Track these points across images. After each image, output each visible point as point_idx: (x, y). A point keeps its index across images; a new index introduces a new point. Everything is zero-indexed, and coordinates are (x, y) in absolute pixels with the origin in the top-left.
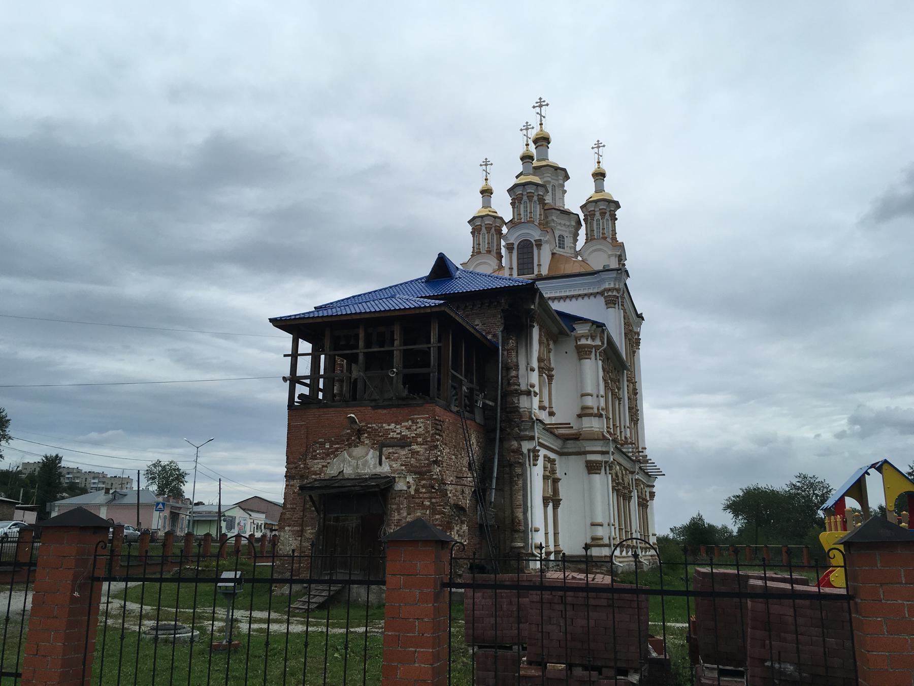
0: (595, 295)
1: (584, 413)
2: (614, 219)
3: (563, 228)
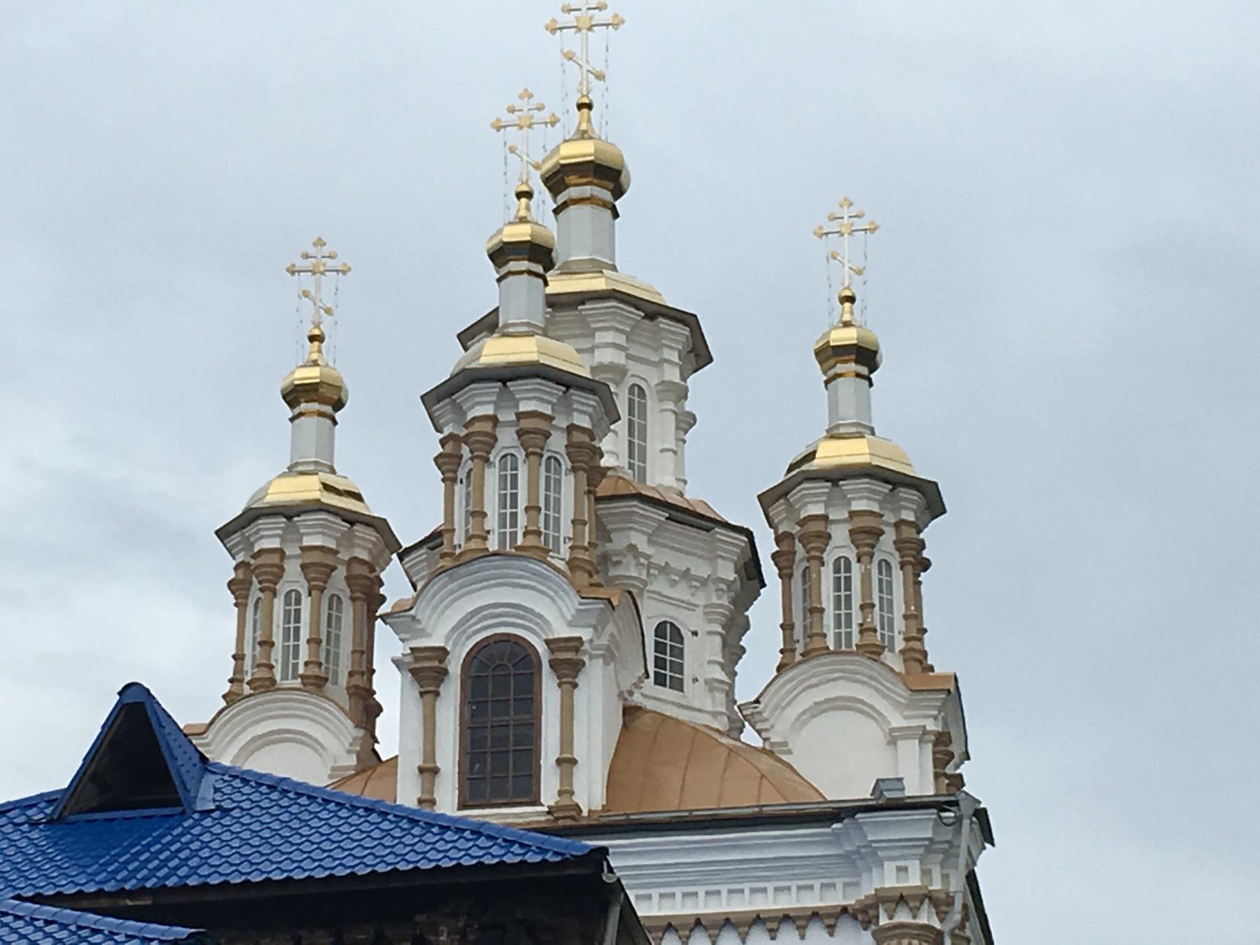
3: (682, 592)
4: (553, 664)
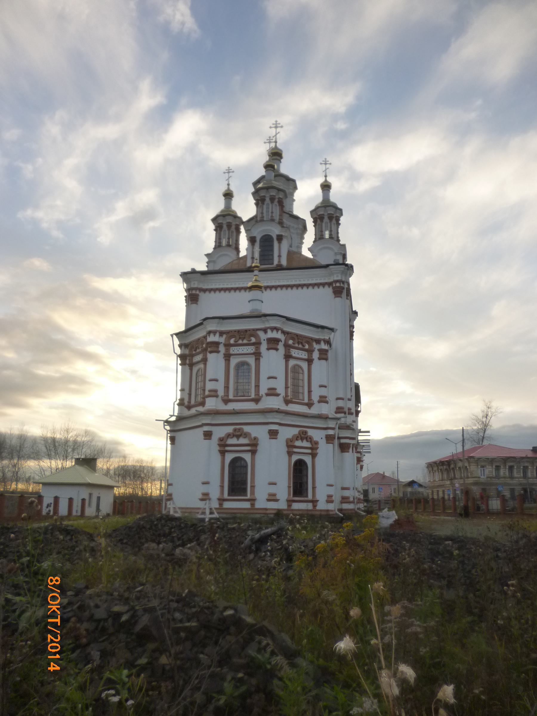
0: (323, 285)
2: (338, 224)
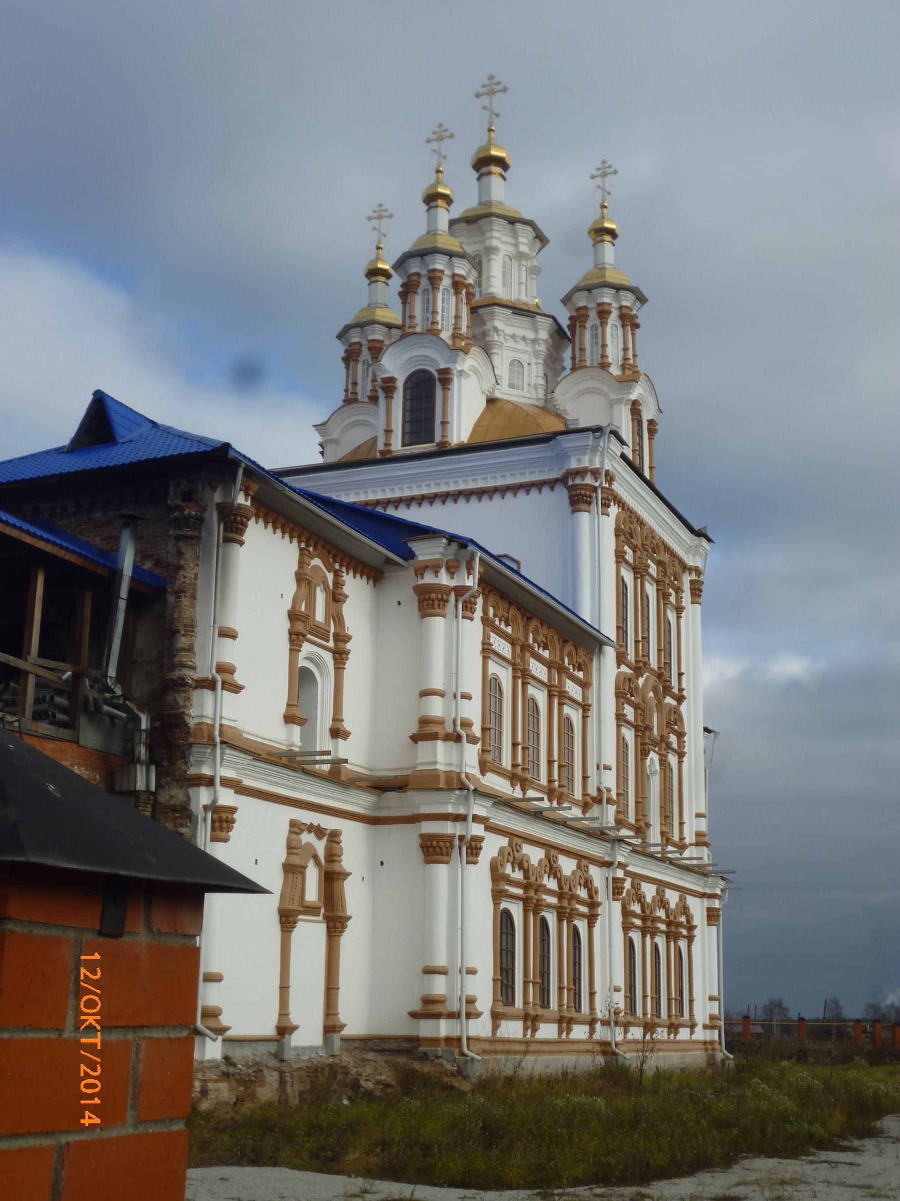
0: (552, 484)
1: (427, 730)
4: (440, 380)
